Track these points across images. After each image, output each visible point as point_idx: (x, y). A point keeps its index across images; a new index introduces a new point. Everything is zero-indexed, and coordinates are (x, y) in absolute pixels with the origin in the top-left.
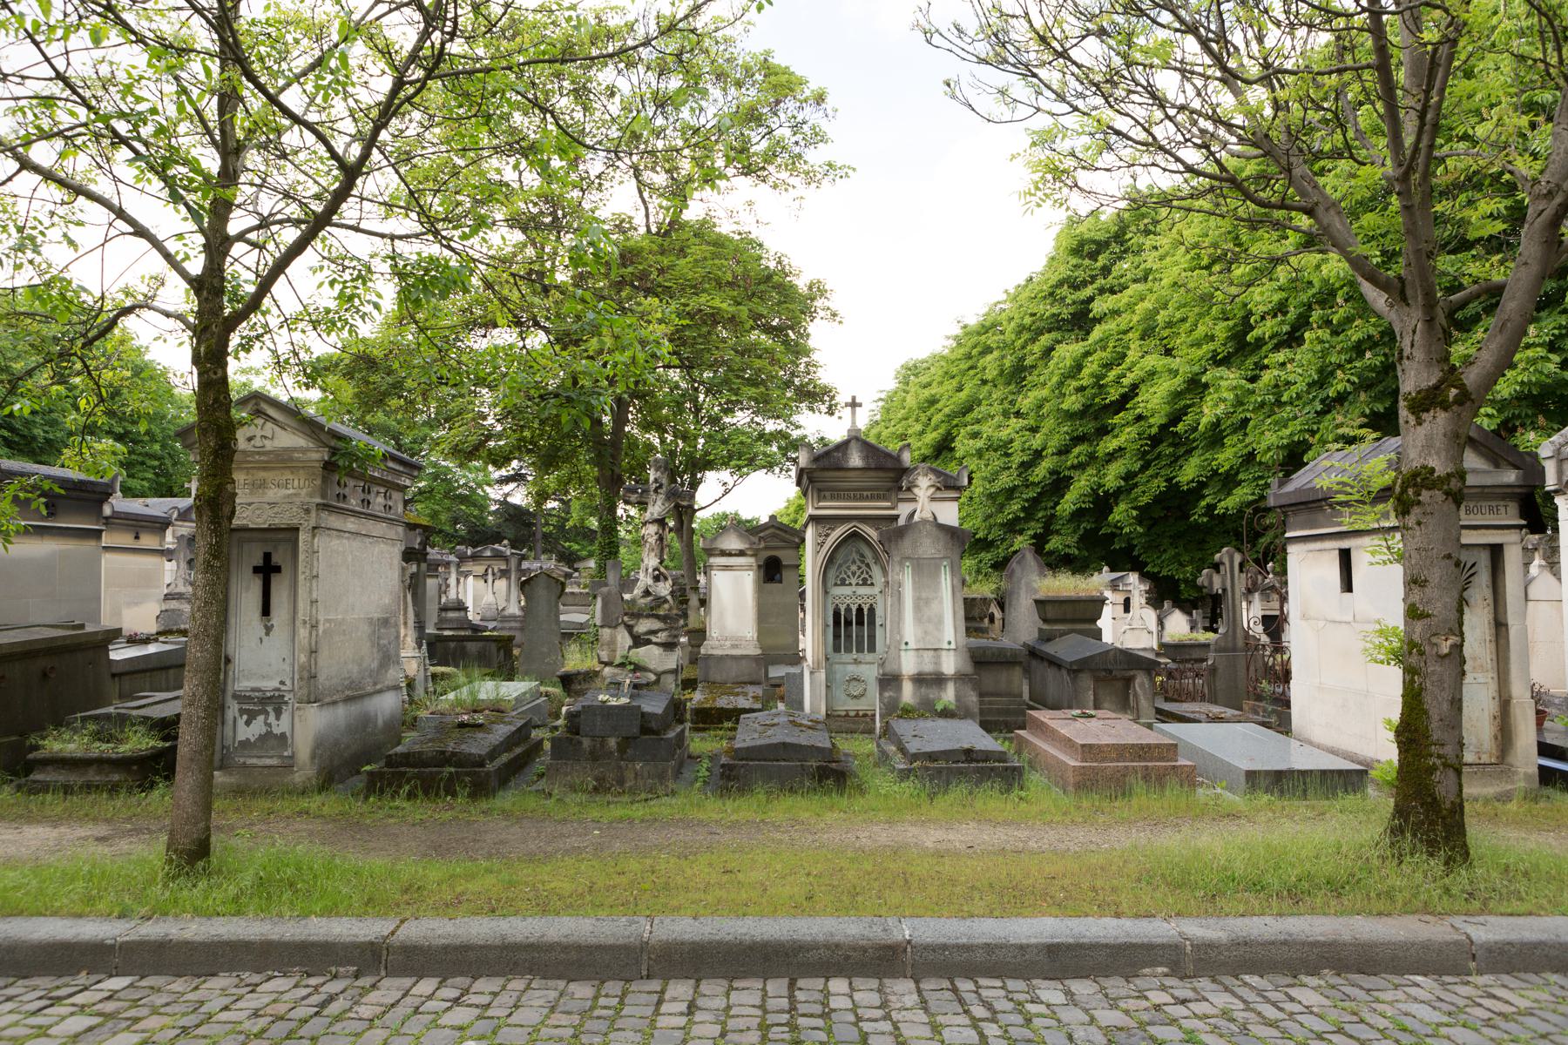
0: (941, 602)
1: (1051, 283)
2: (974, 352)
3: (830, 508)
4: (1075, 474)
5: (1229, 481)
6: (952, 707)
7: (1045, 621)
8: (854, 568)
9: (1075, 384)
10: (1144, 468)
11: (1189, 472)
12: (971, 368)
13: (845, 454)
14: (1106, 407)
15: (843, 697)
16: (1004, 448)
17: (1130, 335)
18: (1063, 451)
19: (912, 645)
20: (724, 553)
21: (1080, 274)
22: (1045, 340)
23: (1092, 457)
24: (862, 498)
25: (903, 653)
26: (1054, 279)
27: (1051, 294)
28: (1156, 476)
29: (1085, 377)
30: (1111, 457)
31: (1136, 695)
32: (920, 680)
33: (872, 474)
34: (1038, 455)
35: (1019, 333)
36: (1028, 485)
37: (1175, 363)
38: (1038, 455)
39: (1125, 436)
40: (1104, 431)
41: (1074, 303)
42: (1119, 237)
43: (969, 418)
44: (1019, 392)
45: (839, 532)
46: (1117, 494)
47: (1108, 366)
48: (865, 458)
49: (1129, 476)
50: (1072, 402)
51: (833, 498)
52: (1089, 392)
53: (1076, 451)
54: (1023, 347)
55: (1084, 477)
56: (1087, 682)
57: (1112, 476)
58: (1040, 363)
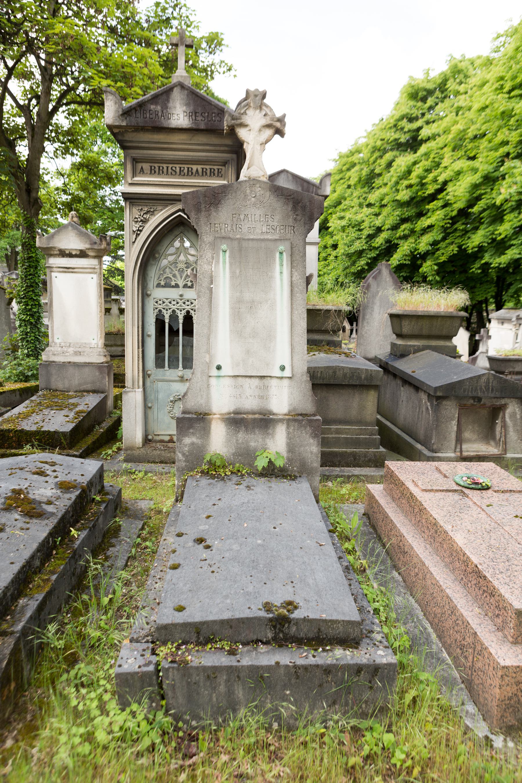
2: (344, 168)
3: (149, 184)
4: (401, 242)
5: (500, 246)
6: (279, 463)
7: (399, 336)
9: (406, 183)
10: (444, 239)
11: (477, 239)
12: (341, 179)
13: (165, 107)
14: (425, 198)
16: (358, 226)
17: (446, 149)
18: (395, 228)
19: (226, 370)
20: (63, 254)
21: (415, 112)
22: (388, 156)
23: (413, 231)
25: (213, 381)
26: (397, 116)
27: (395, 126)
28: (452, 243)
29: (413, 179)
30: (425, 231)
31: (504, 426)
32: (237, 421)
33: (202, 139)
34: (379, 230)
36: (372, 249)
37: (476, 164)
38: (379, 230)
39: (436, 216)
40: (420, 215)
41: (409, 131)
42: (442, 86)
43: (338, 209)
44: (370, 192)
46: (424, 257)
47: (428, 171)
48: (193, 114)
49: (435, 243)
50: (404, 195)
51: (152, 172)
52: (415, 188)
53: (403, 227)
54: (374, 162)
55: (406, 244)
56: (451, 409)
57: (424, 244)
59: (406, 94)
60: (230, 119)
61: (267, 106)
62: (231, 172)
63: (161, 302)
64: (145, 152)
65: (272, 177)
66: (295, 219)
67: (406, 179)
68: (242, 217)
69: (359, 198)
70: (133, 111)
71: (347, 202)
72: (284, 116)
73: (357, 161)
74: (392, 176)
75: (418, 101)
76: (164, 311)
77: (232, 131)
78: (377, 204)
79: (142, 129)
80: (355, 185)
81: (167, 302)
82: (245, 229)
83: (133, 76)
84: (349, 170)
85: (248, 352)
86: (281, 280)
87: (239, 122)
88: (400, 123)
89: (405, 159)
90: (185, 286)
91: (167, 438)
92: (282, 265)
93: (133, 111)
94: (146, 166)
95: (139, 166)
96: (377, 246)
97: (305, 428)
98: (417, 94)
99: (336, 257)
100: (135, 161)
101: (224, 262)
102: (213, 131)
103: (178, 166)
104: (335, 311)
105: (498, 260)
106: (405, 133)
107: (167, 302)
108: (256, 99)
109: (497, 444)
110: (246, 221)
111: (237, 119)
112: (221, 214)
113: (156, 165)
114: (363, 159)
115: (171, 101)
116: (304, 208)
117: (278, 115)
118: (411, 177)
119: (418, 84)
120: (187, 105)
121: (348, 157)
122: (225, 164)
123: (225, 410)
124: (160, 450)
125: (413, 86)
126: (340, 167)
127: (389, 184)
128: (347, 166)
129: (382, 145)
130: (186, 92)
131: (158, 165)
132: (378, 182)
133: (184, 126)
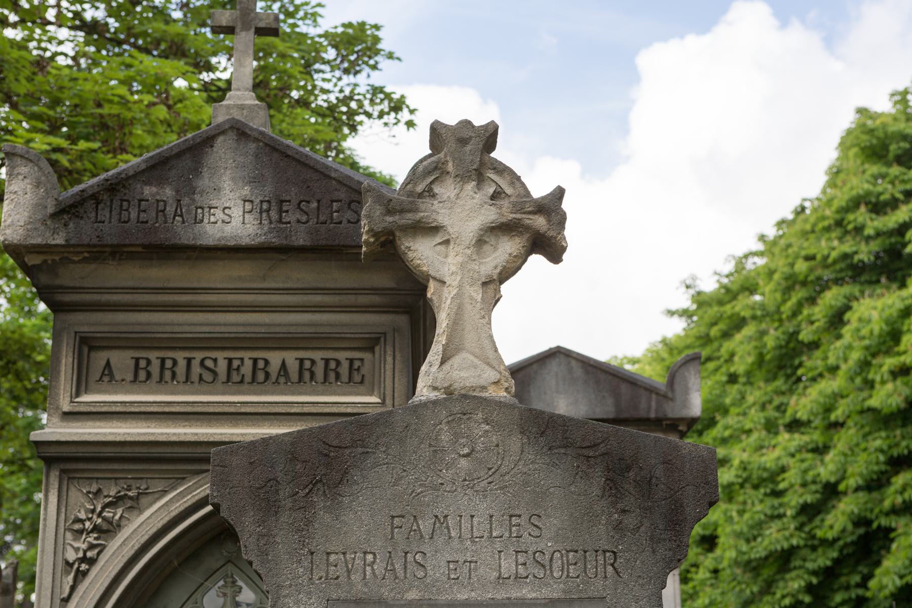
1: (836, 204)
2: (714, 331)
4: (900, 523)
9: (890, 362)
13: (187, 189)
16: (769, 482)
18: (875, 484)
24: (261, 377)
26: (842, 197)
27: (839, 223)
34: (831, 491)
35: (787, 290)
36: (816, 545)
38: (831, 491)
41: (878, 234)
44: (791, 391)
48: (272, 207)
51: (140, 376)
53: (899, 481)
54: (795, 314)
58: (825, 338)
59: (855, 150)
60: (378, 211)
61: (502, 169)
62: (390, 363)
64: (121, 317)
65: (525, 373)
66: (618, 527)
67: (888, 352)
68: (425, 526)
69: (763, 407)
70: (90, 205)
71: (732, 420)
72: (559, 193)
73: (746, 313)
74: (849, 347)
75: (889, 165)
77: (388, 250)
78: (817, 422)
79: (118, 253)
80: (748, 374)
83: (124, 125)
84: (726, 335)
87: (409, 218)
88: (851, 217)
89: (879, 303)
93: (90, 205)
94: (121, 360)
95: (100, 359)
96: (830, 535)
98: (885, 147)
99: (716, 571)
100: (87, 345)
102: (334, 251)
103: (221, 356)
106: (868, 239)
108: (466, 150)
110: (440, 540)
113: (153, 355)
114: (762, 306)
115: (206, 174)
116: (646, 486)
117: (539, 189)
118: (902, 348)
119: (884, 125)
120: (255, 181)
121: (721, 303)
122: (371, 343)
125: (871, 131)
126: (703, 329)
127: (844, 367)
128: (722, 326)
129: (811, 270)
130: (252, 146)
131: (158, 358)
132: (812, 362)
133: (245, 241)
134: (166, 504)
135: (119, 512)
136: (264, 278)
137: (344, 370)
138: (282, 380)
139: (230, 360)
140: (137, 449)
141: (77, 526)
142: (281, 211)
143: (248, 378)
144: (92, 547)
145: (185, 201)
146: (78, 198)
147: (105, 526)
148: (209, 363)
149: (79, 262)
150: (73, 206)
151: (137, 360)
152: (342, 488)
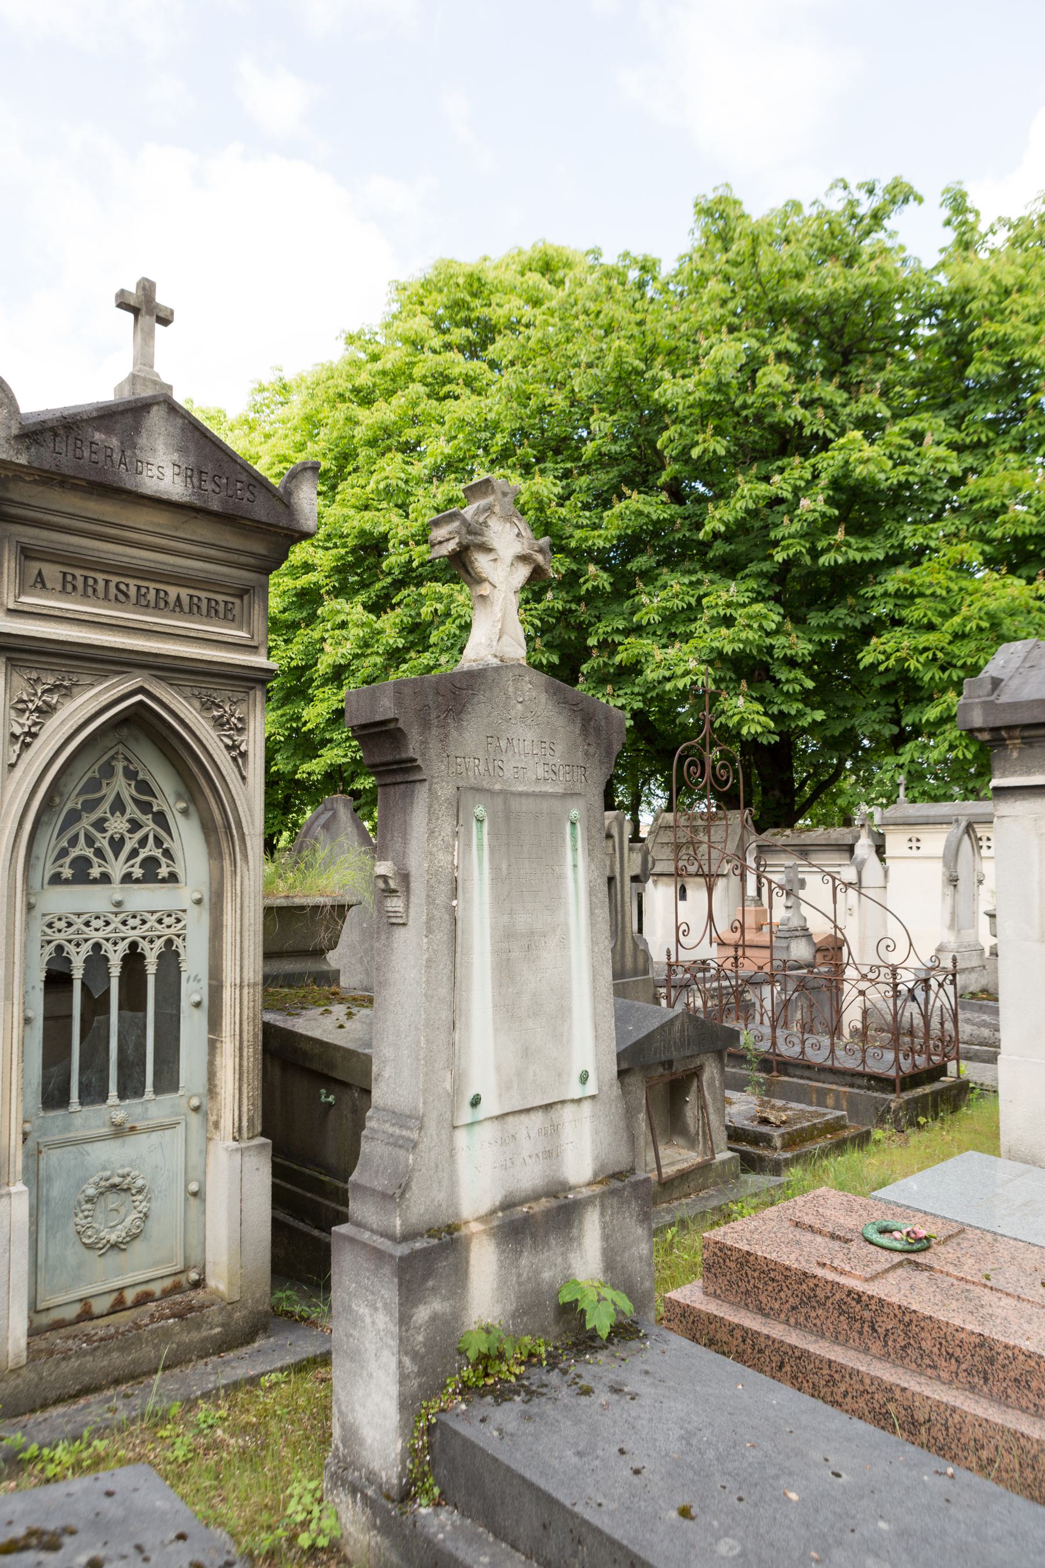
0: (564, 943)
8: (118, 825)
13: (130, 443)
15: (74, 1254)
19: (490, 1107)
24: (160, 605)
33: (204, 531)
45: (88, 703)
48: (195, 473)
51: (67, 588)
63: (62, 924)
64: (55, 536)
66: (587, 754)
68: (503, 744)
76: (71, 948)
81: (79, 922)
82: (508, 773)
85: (526, 1053)
86: (576, 881)
87: (479, 540)
90: (127, 878)
91: (72, 1312)
92: (575, 850)
93: (49, 435)
94: (52, 572)
95: (35, 567)
97: (629, 1203)
101: (480, 846)
103: (132, 582)
104: (333, 906)
105: (306, 767)
107: (79, 922)
109: (692, 1144)
110: (510, 753)
111: (475, 534)
112: (467, 735)
113: (78, 573)
116: (598, 730)
120: (182, 450)
123: (485, 1207)
124: (81, 1353)
133: (175, 498)
134: (96, 695)
135: (56, 697)
136: (177, 530)
137: (221, 608)
138: (178, 609)
139: (139, 587)
140: (75, 649)
141: (21, 706)
142: (201, 480)
143: (152, 604)
144: (35, 724)
145: (128, 453)
146: (39, 427)
147: (45, 708)
148: (123, 587)
149: (29, 482)
150: (35, 433)
151: (65, 574)
152: (463, 715)
